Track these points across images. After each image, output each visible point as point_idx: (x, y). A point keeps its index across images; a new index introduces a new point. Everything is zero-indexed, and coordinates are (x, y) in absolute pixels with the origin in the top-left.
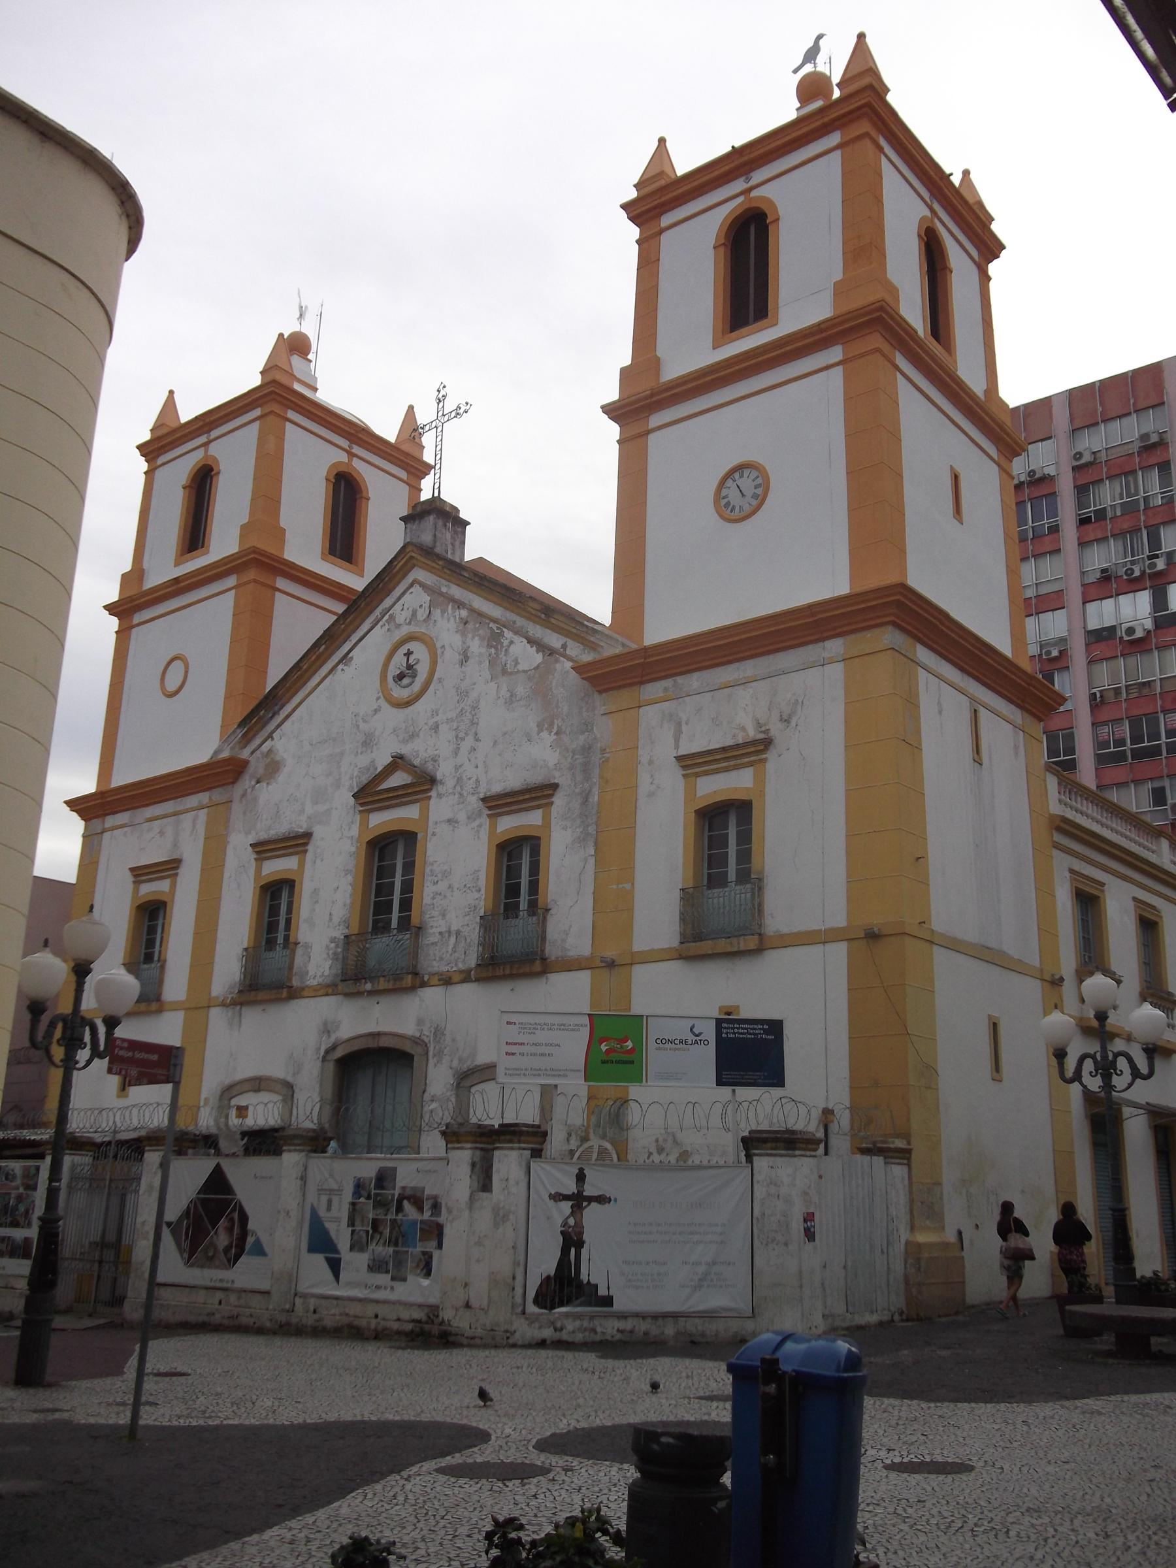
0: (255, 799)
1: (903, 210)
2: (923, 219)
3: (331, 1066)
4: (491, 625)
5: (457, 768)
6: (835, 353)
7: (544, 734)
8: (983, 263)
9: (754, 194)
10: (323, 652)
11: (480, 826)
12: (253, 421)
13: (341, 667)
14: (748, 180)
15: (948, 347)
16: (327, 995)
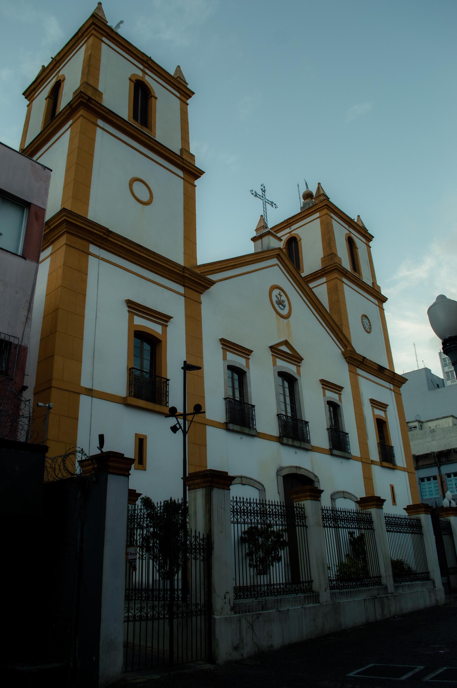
1: (340, 232)
2: (347, 234)
3: (281, 479)
6: (324, 280)
8: (367, 243)
9: (292, 233)
14: (290, 229)
15: (360, 273)
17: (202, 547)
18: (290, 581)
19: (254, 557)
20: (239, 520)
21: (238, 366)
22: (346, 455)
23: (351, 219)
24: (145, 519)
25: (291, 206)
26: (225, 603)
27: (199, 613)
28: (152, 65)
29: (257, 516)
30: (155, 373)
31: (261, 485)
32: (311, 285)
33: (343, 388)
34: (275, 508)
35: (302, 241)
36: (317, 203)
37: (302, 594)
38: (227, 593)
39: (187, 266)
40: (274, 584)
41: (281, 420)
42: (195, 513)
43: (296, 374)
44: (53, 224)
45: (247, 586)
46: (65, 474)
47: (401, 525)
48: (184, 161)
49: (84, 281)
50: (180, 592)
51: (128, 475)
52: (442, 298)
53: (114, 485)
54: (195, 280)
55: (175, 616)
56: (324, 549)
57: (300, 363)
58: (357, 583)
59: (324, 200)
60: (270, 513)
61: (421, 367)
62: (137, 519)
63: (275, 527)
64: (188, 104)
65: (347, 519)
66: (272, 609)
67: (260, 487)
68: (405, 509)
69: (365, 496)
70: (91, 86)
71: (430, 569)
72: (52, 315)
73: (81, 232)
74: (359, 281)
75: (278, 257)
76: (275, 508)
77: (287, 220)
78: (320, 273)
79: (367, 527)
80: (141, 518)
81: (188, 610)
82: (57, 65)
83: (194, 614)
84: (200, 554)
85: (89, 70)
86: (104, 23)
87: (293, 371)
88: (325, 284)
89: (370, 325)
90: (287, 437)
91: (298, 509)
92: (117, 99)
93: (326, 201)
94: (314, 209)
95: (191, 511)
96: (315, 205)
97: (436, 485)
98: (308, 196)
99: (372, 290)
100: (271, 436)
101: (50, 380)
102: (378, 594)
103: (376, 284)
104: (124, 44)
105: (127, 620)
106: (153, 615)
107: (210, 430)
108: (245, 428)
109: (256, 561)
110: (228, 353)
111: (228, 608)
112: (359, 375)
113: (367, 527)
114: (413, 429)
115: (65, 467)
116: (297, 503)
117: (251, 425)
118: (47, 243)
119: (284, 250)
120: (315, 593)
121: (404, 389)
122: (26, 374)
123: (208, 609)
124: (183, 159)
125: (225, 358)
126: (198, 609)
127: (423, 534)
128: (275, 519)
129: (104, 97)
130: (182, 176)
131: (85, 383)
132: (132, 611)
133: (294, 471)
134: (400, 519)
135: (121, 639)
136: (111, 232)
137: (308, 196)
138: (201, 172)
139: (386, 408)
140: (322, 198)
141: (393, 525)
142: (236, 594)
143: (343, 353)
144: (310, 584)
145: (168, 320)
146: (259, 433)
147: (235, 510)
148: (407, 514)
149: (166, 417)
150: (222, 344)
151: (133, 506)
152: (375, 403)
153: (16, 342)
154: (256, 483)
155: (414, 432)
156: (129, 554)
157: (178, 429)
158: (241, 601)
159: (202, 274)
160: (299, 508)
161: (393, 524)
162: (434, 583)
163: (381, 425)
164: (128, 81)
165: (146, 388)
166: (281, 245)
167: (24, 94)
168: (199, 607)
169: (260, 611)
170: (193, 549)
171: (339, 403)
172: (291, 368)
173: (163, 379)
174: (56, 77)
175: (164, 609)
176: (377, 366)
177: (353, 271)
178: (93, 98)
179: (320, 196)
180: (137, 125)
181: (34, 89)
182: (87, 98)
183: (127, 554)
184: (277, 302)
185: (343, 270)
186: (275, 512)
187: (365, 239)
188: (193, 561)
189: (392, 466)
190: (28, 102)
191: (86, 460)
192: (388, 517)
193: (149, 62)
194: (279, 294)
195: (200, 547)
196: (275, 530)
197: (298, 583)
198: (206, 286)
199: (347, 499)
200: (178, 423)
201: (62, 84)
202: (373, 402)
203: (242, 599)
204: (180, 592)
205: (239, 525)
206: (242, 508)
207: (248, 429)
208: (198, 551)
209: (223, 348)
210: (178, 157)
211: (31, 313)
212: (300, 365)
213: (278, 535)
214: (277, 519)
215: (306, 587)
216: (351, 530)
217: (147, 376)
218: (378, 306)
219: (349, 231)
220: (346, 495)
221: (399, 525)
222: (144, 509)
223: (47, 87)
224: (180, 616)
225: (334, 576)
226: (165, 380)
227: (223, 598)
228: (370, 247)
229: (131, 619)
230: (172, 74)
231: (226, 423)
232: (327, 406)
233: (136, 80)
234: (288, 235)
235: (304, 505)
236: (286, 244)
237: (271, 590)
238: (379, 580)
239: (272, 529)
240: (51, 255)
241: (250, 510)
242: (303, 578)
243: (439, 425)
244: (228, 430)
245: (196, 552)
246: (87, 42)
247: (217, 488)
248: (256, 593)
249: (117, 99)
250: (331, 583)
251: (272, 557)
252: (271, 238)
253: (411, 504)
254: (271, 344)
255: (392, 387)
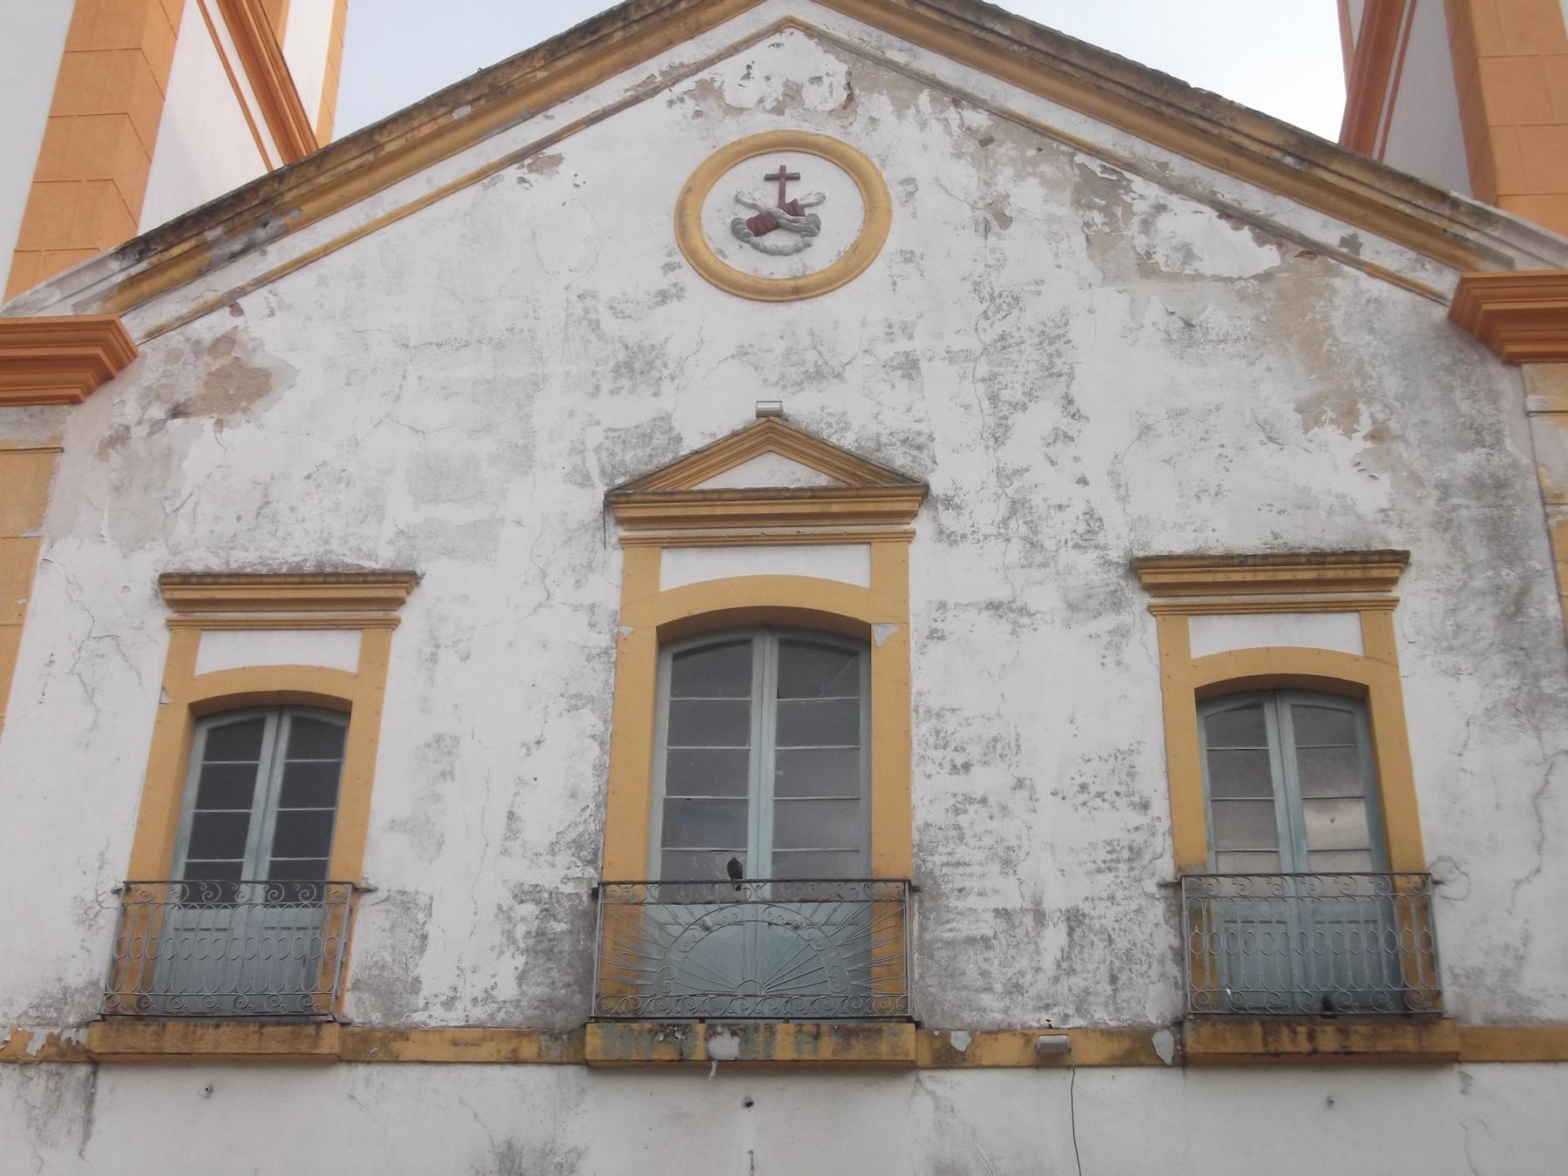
0: (167, 457)
4: (1081, 158)
5: (1004, 476)
7: (1329, 433)
10: (458, 125)
11: (1123, 632)
13: (512, 172)
16: (516, 1061)
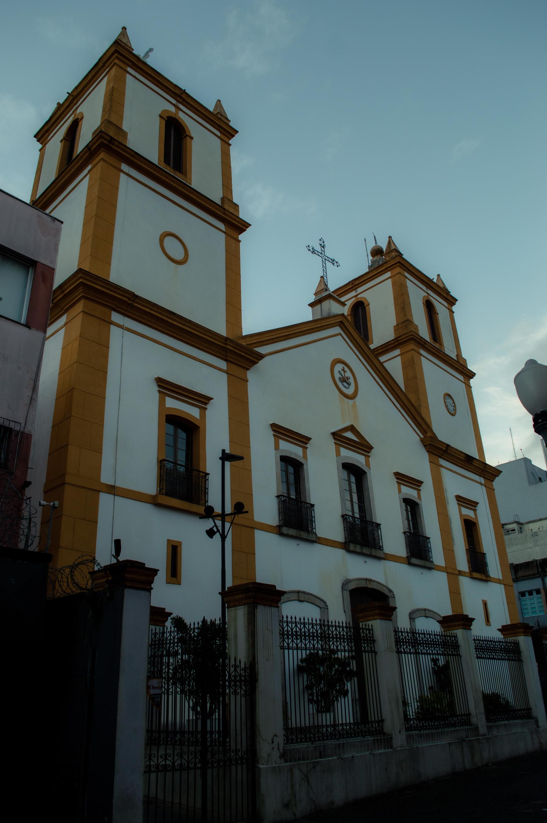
1: (416, 295)
3: (347, 594)
6: (397, 352)
8: (450, 307)
9: (359, 296)
12: (61, 328)
15: (441, 344)
17: (243, 679)
18: (359, 721)
19: (315, 691)
20: (291, 645)
21: (293, 456)
22: (428, 564)
23: (430, 279)
24: (176, 644)
25: (357, 264)
26: (273, 748)
27: (239, 762)
28: (187, 99)
29: (344, 642)
30: (192, 466)
31: (322, 602)
32: (382, 359)
33: (423, 482)
34: (336, 629)
35: (370, 306)
36: (388, 260)
37: (371, 737)
38: (276, 736)
39: (230, 337)
40: (327, 726)
41: (347, 521)
42: (236, 637)
43: (365, 466)
44: (68, 288)
45: (301, 727)
46: (74, 589)
47: (494, 650)
48: (226, 212)
49: (106, 356)
50: (199, 736)
51: (150, 590)
52: (531, 364)
53: (132, 600)
54: (239, 353)
55: (210, 766)
56: (400, 680)
57: (369, 452)
58: (440, 723)
59: (396, 256)
60: (336, 636)
61: (519, 457)
62: (166, 644)
63: (339, 653)
64: (230, 145)
65: (427, 644)
66: (332, 756)
67: (322, 605)
68: (499, 630)
69: (451, 614)
70: (114, 124)
71: (532, 705)
72: (66, 396)
73: (98, 295)
74: (440, 353)
75: (341, 325)
76: (336, 629)
77: (352, 281)
78: (392, 344)
79: (452, 652)
80: (170, 643)
81: (214, 760)
82: (75, 102)
83: (234, 762)
84: (241, 688)
85: (111, 106)
86: (130, 51)
87: (361, 463)
88: (399, 357)
89: (455, 406)
90: (355, 542)
91: (365, 631)
92: (145, 138)
93: (398, 258)
94: (384, 268)
95: (231, 634)
96: (386, 263)
97: (540, 600)
98: (377, 252)
99: (456, 364)
100: (335, 542)
101: (63, 475)
102: (467, 736)
103: (461, 356)
104: (152, 74)
105: (148, 770)
106: (181, 764)
107: (260, 536)
108: (302, 533)
109: (317, 696)
110: (280, 441)
111: (276, 754)
112: (442, 466)
113: (452, 652)
114: (510, 532)
115: (74, 579)
116: (364, 623)
117: (310, 529)
118: (60, 311)
119: (349, 318)
120: (387, 736)
121: (497, 483)
122: (29, 466)
123: (251, 756)
124: (225, 209)
125: (277, 447)
126: (238, 757)
127: (522, 661)
128: (335, 643)
129: (129, 137)
130: (224, 230)
131: (106, 478)
132: (155, 759)
133: (363, 584)
134: (494, 642)
135: (140, 795)
136: (137, 297)
137: (377, 252)
138: (247, 225)
139: (476, 507)
140: (394, 254)
141: (485, 649)
142: (287, 738)
143: (422, 440)
144: (381, 724)
145: (307, 442)
146: (319, 538)
147: (286, 633)
148: (502, 636)
149: (200, 518)
150: (273, 430)
151: (161, 628)
152: (462, 501)
153: (17, 428)
154: (316, 599)
155: (512, 536)
156: (151, 687)
157: (214, 533)
158: (292, 746)
159: (248, 346)
160: (366, 630)
161: (485, 648)
162: (537, 721)
163: (470, 527)
164: (158, 119)
165: (179, 484)
166: (346, 310)
167: (35, 136)
168: (240, 753)
169: (317, 759)
170: (232, 681)
171: (418, 501)
172: (358, 459)
173: (201, 474)
174: (73, 116)
175: (195, 756)
176: (464, 455)
177: (432, 341)
178: (116, 138)
179: (391, 251)
180: (169, 170)
181: (48, 131)
182: (109, 138)
183: (148, 687)
184: (340, 379)
185: (420, 340)
186: (336, 635)
187: (447, 302)
188: (233, 697)
189: (484, 578)
190: (41, 146)
191: (99, 571)
192: (478, 640)
193: (184, 96)
194: (343, 370)
195: (240, 678)
196: (340, 656)
197: (367, 724)
198: (254, 361)
199: (305, 603)
200: (216, 525)
201: (80, 123)
202: (460, 499)
203: (294, 743)
204: (199, 736)
205: (291, 651)
206: (294, 630)
207: (306, 533)
208: (238, 683)
209: (274, 435)
210: (218, 207)
211: (37, 393)
212: (370, 455)
213: (344, 663)
214: (338, 643)
215: (376, 728)
216: (437, 656)
217: (182, 469)
218: (464, 383)
219: (427, 293)
220: (428, 614)
221: (493, 650)
222: (174, 632)
223: (63, 127)
224: (215, 765)
225: (414, 714)
226: (204, 474)
227: (270, 742)
228: (453, 312)
229: (153, 769)
230: (212, 111)
231: (279, 527)
232: (404, 504)
233: (168, 117)
234: (354, 299)
235: (372, 626)
236: (351, 311)
237: (337, 732)
238: (467, 718)
239: (336, 656)
240: (65, 325)
241: (305, 632)
242: (372, 717)
243: (543, 527)
244: (281, 534)
245: (235, 685)
246: (109, 73)
247: (262, 605)
248: (312, 735)
249: (145, 138)
250: (408, 723)
251: (336, 691)
252: (332, 302)
253: (509, 623)
254: (334, 430)
255: (482, 480)
